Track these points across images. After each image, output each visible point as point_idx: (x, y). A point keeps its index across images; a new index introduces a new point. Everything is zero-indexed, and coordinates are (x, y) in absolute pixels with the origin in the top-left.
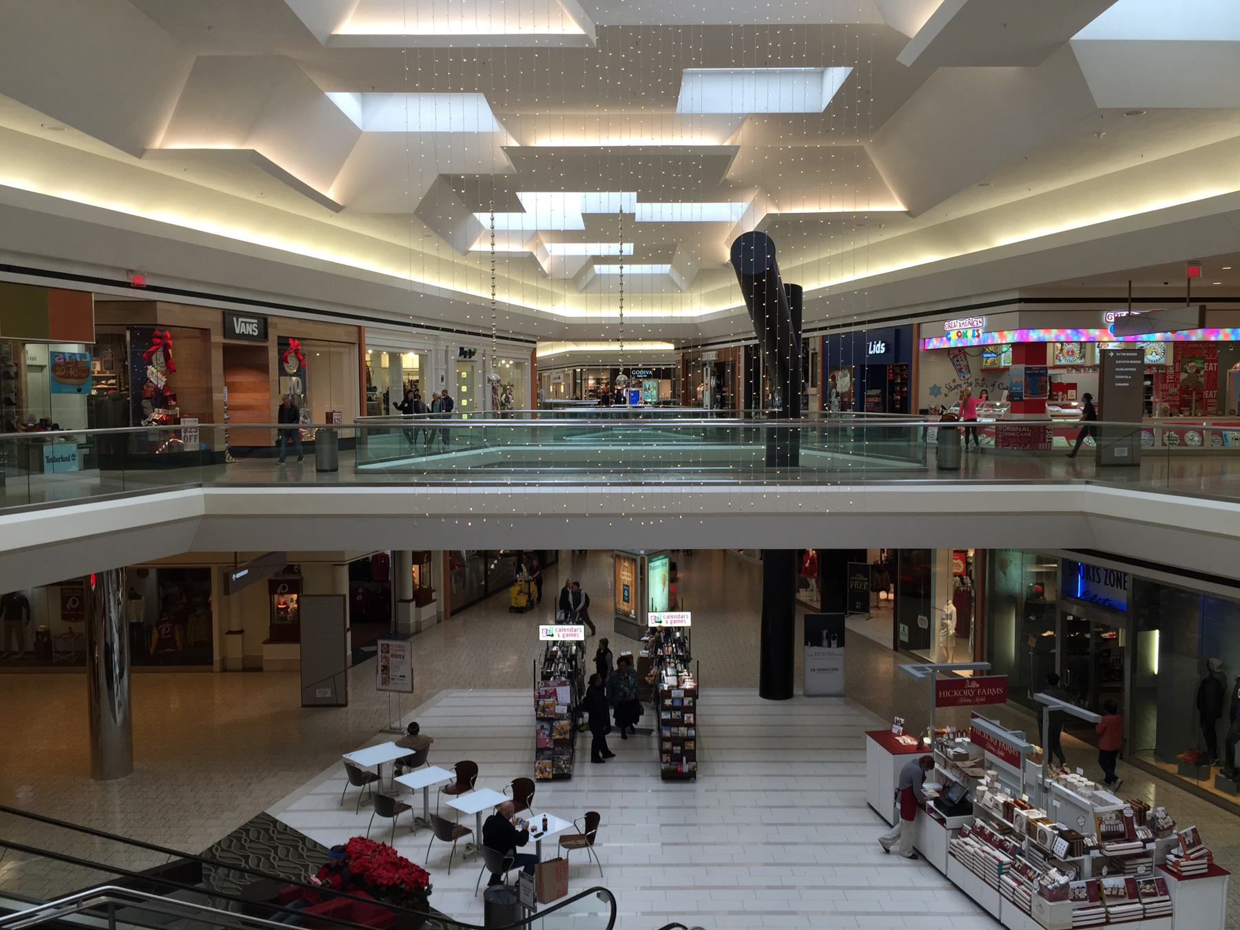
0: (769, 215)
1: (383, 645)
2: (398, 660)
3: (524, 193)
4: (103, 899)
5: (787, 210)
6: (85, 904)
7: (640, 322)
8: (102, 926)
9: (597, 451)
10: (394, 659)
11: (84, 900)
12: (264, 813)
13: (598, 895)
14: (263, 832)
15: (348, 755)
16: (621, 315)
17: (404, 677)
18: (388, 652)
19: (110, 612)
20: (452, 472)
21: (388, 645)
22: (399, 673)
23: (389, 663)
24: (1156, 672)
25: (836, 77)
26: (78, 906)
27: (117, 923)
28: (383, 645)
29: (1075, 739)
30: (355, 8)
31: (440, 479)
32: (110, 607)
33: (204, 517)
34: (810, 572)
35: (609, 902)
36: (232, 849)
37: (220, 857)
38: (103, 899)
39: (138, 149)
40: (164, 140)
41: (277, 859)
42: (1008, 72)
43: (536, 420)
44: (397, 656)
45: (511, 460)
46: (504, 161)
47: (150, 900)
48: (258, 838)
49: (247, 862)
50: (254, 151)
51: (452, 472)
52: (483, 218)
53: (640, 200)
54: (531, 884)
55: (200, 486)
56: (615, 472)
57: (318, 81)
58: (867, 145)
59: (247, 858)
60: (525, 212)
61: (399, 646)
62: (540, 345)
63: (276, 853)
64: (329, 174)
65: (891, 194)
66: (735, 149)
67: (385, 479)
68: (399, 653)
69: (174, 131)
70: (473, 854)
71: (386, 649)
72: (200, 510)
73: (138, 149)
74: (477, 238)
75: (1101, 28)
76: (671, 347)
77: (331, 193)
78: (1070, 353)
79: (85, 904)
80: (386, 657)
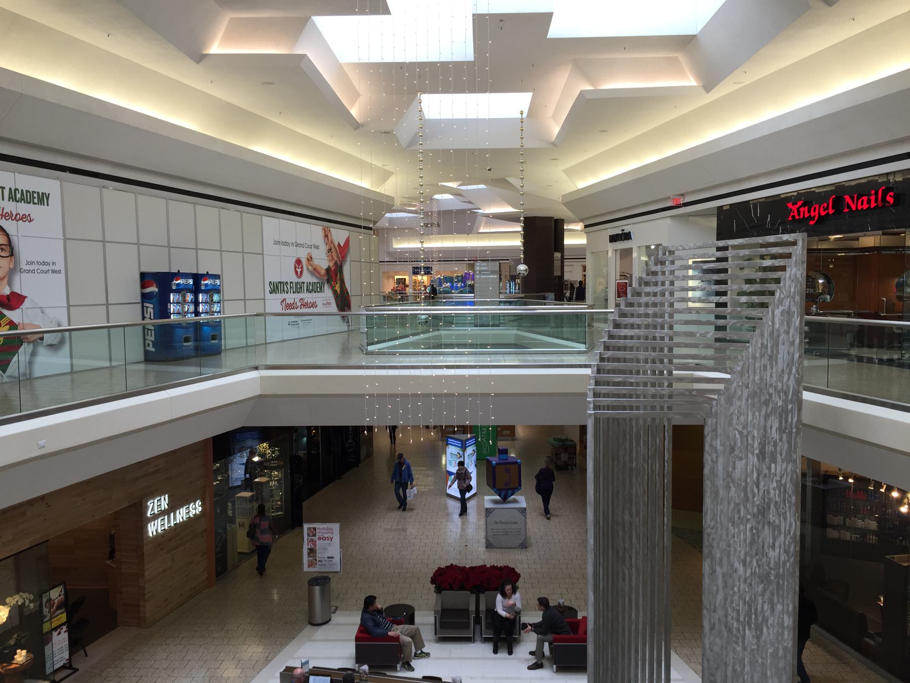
1: (309, 529)
2: (326, 542)
8: (881, 95)
10: (321, 542)
17: (333, 558)
18: (315, 535)
21: (315, 529)
22: (326, 555)
23: (315, 546)
24: (171, 294)
28: (309, 529)
29: (297, 131)
30: (483, 224)
33: (260, 396)
34: (468, 271)
44: (324, 539)
60: (390, 14)
61: (327, 529)
67: (598, 436)
68: (326, 535)
71: (313, 533)
78: (564, 457)
80: (312, 540)
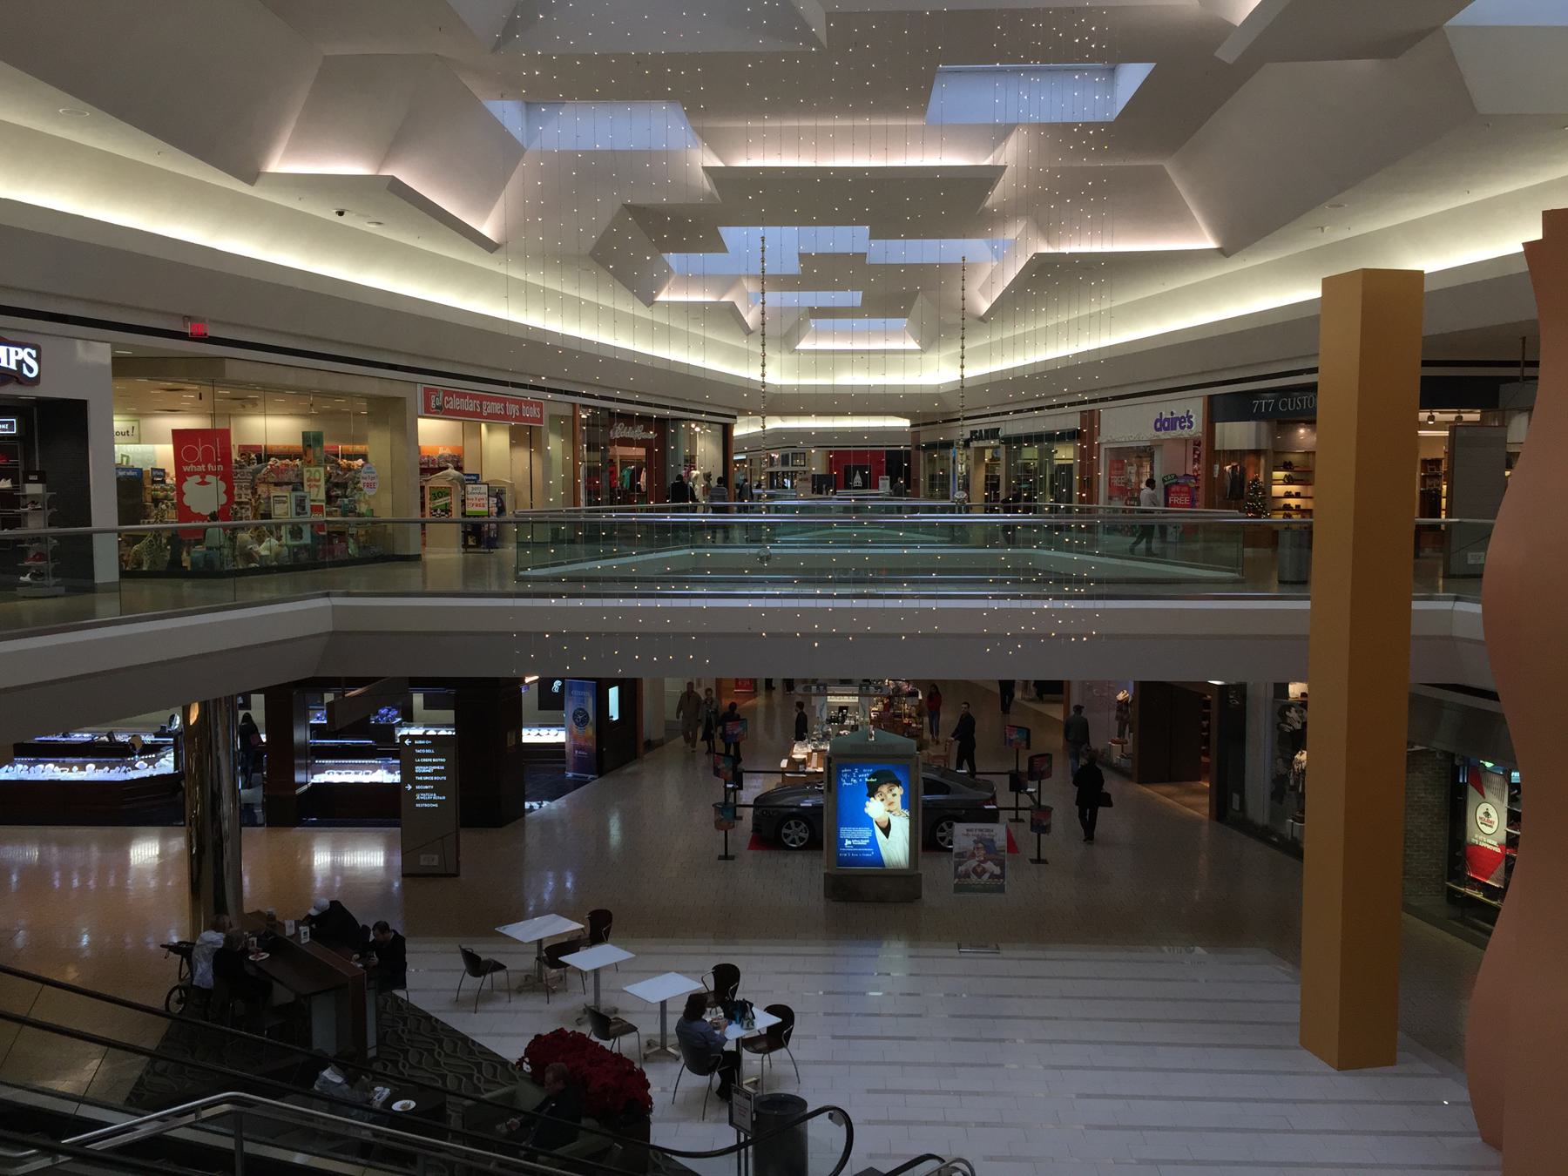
0: (1039, 256)
3: (732, 229)
4: (226, 1107)
5: (1067, 248)
6: (206, 1113)
7: (850, 392)
9: (935, 555)
11: (204, 1109)
12: (717, 1092)
13: (831, 1117)
14: (460, 1043)
15: (502, 928)
16: (962, 376)
19: (218, 748)
20: (632, 580)
25: (1133, 76)
26: (196, 1116)
27: (245, 1143)
31: (619, 588)
32: (217, 742)
33: (332, 633)
35: (844, 1126)
36: (424, 1066)
37: (409, 1075)
38: (226, 1107)
39: (251, 174)
40: (279, 164)
41: (483, 1079)
42: (1363, 66)
43: (918, 515)
45: (1053, 570)
46: (706, 184)
47: (261, 1105)
48: (455, 1051)
49: (444, 1083)
50: (393, 177)
51: (632, 580)
52: (672, 258)
53: (874, 235)
54: (748, 1102)
55: (328, 595)
56: (995, 581)
57: (473, 84)
58: (1169, 166)
59: (444, 1077)
60: (724, 250)
62: (740, 420)
63: (480, 1072)
64: (484, 205)
65: (1200, 229)
66: (996, 172)
69: (295, 149)
70: (656, 1053)
72: (326, 626)
73: (251, 174)
74: (665, 285)
75: (1463, 18)
76: (906, 423)
77: (488, 228)
79: (206, 1113)
